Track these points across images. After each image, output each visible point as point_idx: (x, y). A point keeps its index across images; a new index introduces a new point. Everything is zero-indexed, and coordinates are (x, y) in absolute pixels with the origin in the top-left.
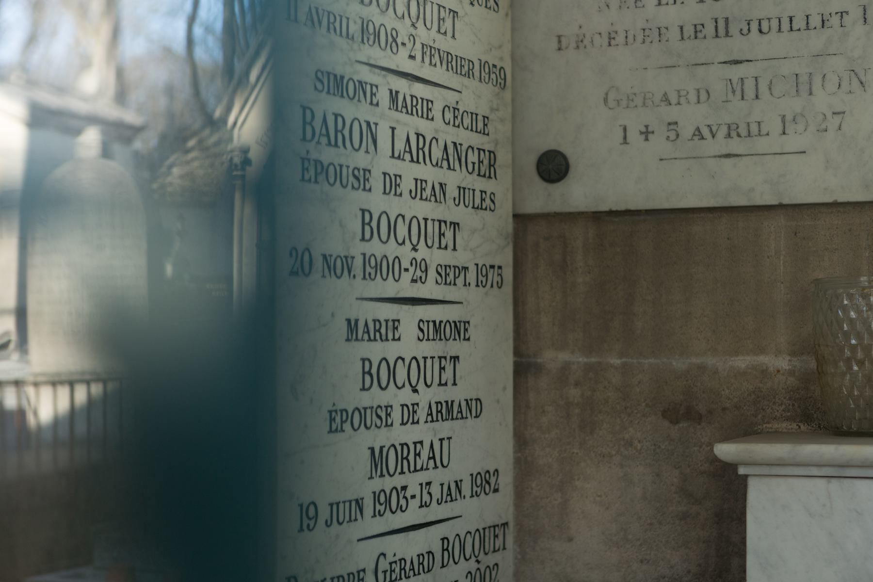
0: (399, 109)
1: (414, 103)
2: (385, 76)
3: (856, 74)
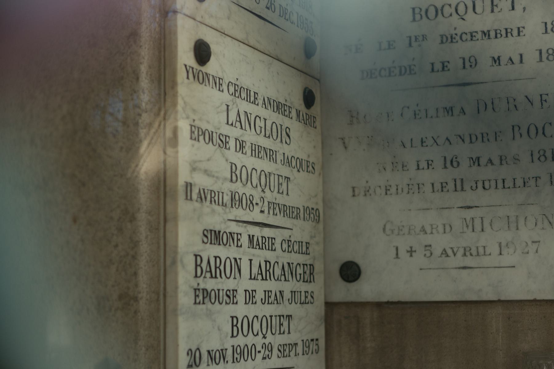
0: (255, 247)
1: (264, 241)
2: (245, 227)
3: (547, 217)
